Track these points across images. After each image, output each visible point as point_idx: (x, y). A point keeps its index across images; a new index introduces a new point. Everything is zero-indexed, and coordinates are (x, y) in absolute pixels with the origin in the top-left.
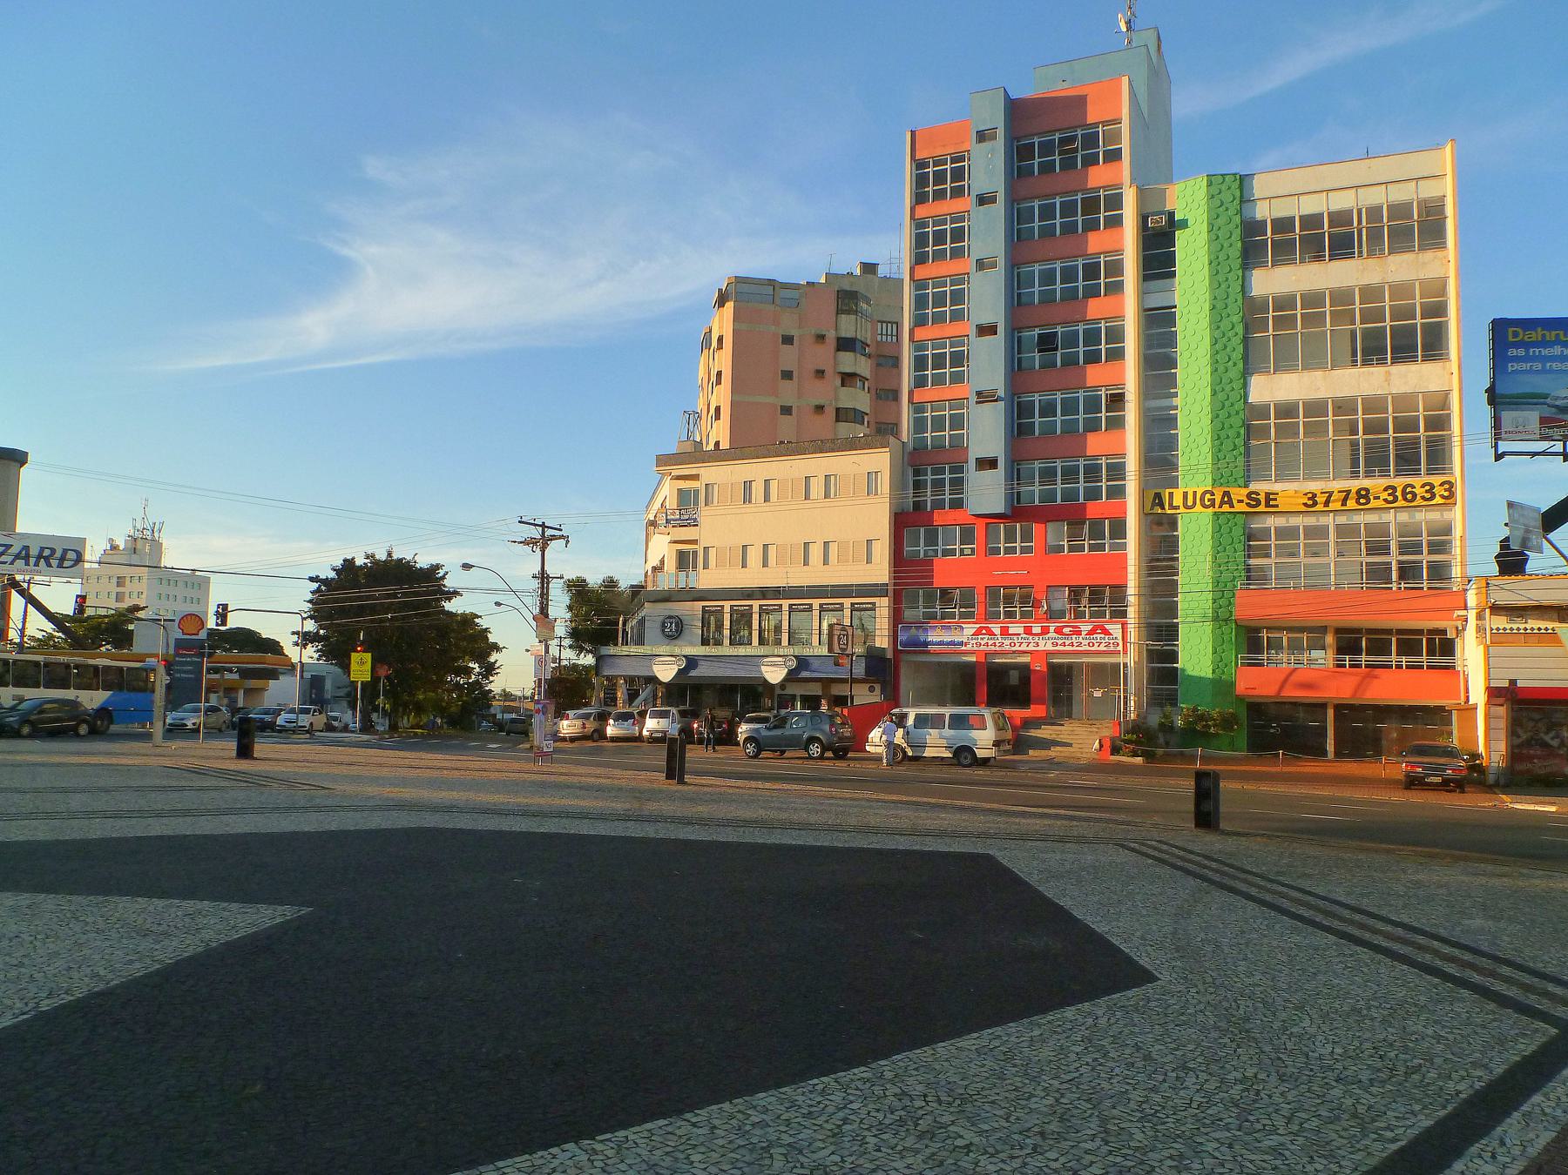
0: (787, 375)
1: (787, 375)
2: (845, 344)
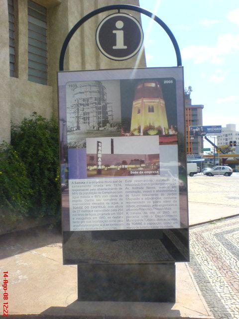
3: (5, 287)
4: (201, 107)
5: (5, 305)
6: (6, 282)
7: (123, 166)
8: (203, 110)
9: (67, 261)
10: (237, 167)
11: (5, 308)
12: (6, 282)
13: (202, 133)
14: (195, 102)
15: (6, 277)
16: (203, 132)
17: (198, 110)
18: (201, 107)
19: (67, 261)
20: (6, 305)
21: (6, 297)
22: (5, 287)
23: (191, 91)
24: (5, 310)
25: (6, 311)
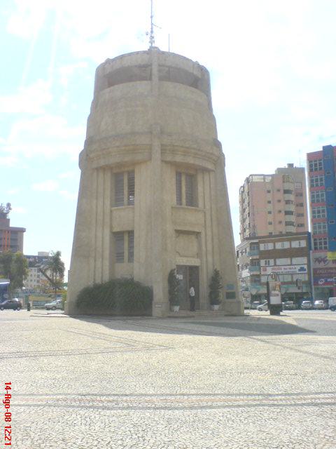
0: (269, 202)
1: (269, 202)
2: (286, 192)
3: (7, 404)
4: (22, 230)
5: (9, 442)
6: (8, 397)
7: (312, 283)
8: (24, 233)
9: (19, 232)
10: (332, 301)
11: (7, 433)
12: (8, 397)
13: (37, 264)
14: (13, 224)
15: (9, 390)
16: (38, 263)
17: (19, 233)
18: (22, 230)
19: (19, 232)
20: (9, 430)
21: (8, 417)
22: (7, 404)
23: (10, 209)
24: (7, 436)
25: (9, 437)
